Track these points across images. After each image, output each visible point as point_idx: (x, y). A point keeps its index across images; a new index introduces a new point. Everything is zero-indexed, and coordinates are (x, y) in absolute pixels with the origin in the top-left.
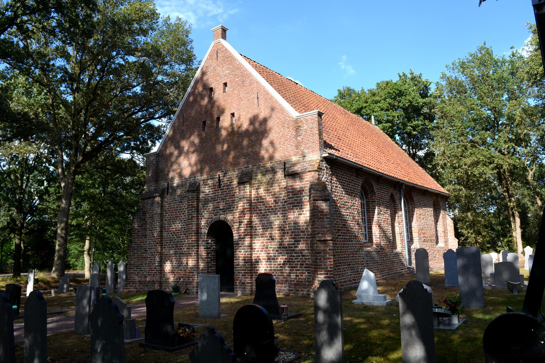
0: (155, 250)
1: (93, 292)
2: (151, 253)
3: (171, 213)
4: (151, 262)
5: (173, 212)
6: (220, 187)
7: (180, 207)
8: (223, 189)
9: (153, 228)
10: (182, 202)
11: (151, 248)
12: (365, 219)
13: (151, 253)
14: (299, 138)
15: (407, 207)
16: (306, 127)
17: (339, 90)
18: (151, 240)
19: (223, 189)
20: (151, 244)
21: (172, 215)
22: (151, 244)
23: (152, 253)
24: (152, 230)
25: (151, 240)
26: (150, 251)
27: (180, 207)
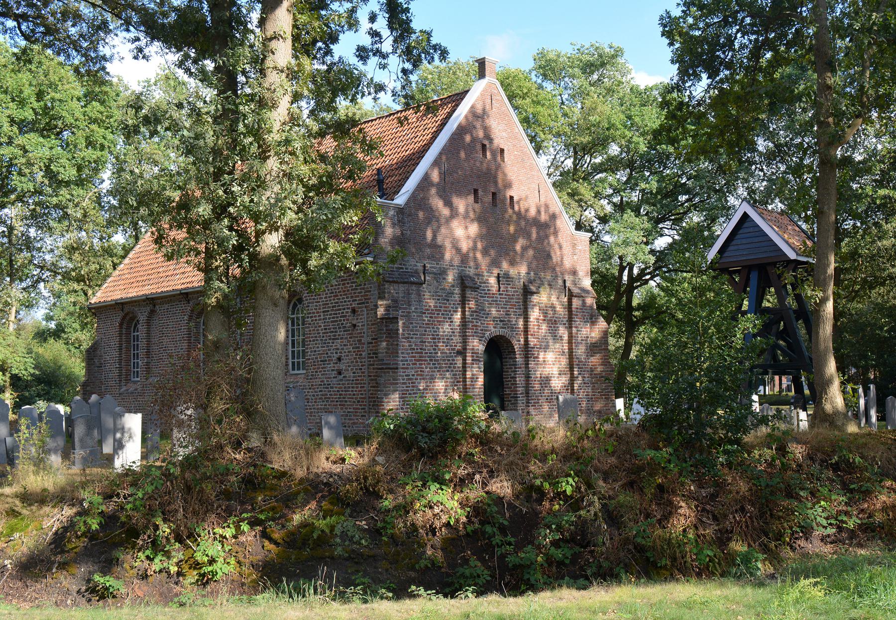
0: (413, 371)
1: (767, 388)
2: (406, 376)
3: (431, 313)
4: (408, 390)
5: (434, 314)
6: (499, 291)
7: (445, 307)
8: (502, 294)
9: (410, 334)
10: (448, 300)
11: (407, 368)
12: (134, 341)
13: (406, 376)
14: (575, 257)
15: (125, 326)
16: (580, 248)
17: (527, 197)
18: (407, 354)
19: (502, 294)
20: (407, 361)
21: (431, 317)
22: (407, 361)
23: (409, 375)
24: (408, 338)
25: (407, 354)
26: (405, 372)
27: (445, 307)
